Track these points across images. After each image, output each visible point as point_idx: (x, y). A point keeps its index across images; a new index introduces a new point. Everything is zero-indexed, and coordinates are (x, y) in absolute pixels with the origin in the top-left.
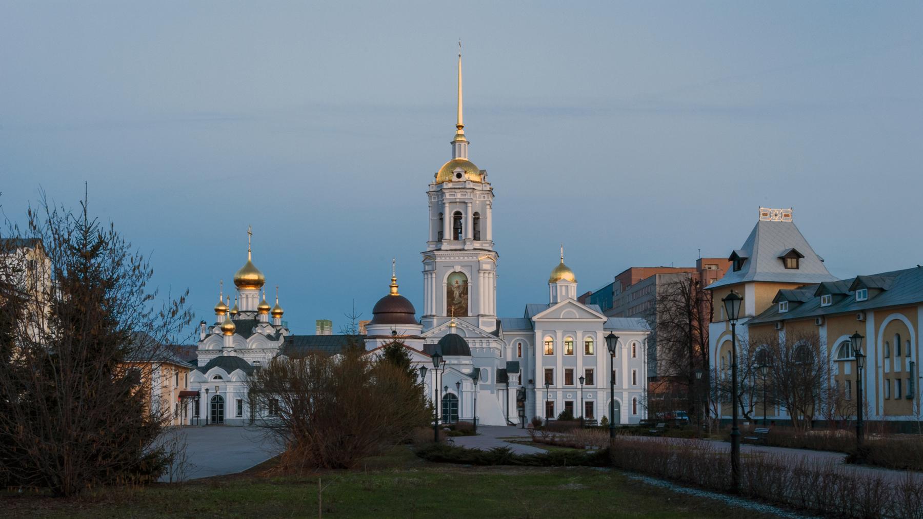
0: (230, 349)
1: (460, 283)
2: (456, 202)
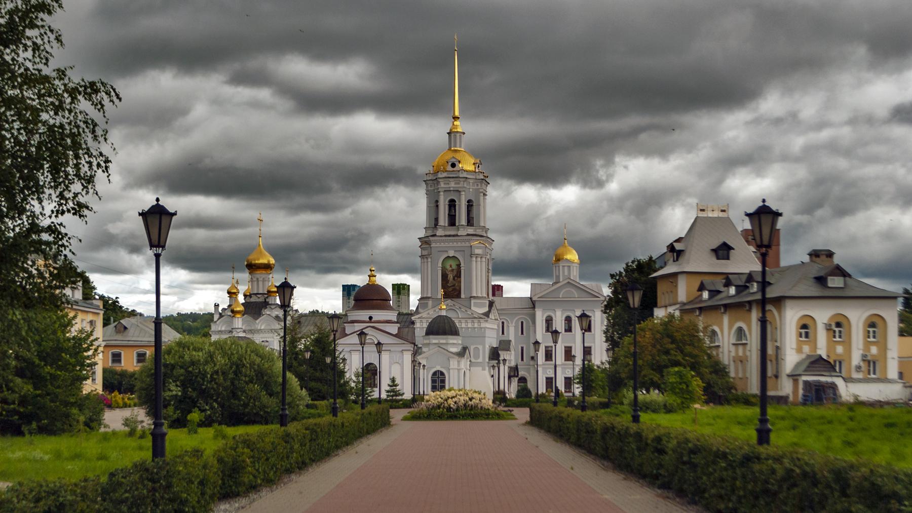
0: (238, 330)
1: (454, 267)
2: (450, 191)
